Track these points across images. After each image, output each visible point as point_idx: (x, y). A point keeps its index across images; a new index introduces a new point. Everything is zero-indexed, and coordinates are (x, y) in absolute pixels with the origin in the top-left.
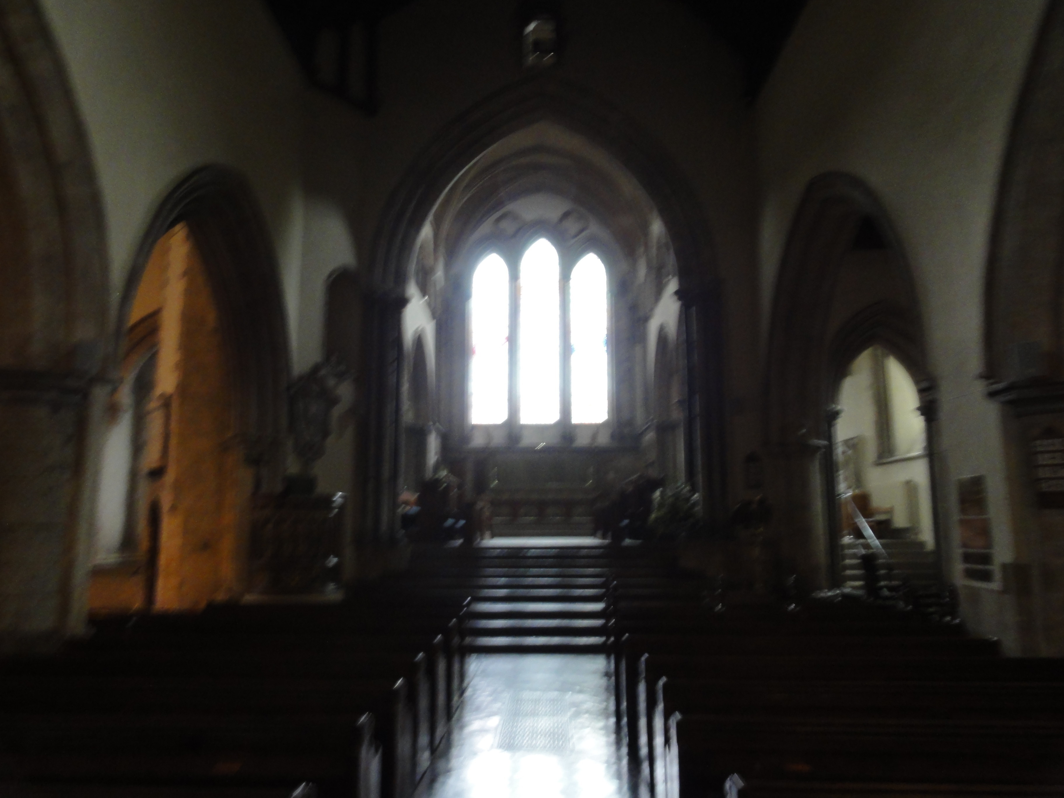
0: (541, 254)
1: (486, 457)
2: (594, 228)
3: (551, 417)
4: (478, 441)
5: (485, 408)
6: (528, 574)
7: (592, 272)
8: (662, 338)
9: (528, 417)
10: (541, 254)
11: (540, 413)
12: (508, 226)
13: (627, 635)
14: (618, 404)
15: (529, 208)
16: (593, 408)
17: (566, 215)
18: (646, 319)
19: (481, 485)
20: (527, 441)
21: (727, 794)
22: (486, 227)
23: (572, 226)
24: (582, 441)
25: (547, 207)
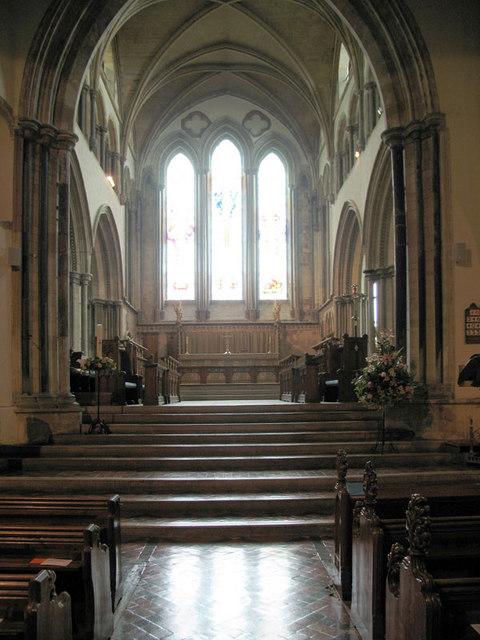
0: (226, 155)
1: (176, 330)
2: (277, 126)
3: (237, 294)
4: (170, 317)
5: (178, 284)
6: (425, 155)
7: (274, 171)
8: (348, 214)
9: (218, 294)
10: (226, 155)
11: (227, 288)
12: (195, 125)
13: (336, 381)
14: (297, 287)
15: (216, 108)
16: (276, 283)
17: (249, 116)
18: (325, 211)
19: (172, 350)
20: (217, 316)
21: (365, 620)
22: (175, 126)
23: (256, 124)
24: (267, 316)
25: (235, 108)
